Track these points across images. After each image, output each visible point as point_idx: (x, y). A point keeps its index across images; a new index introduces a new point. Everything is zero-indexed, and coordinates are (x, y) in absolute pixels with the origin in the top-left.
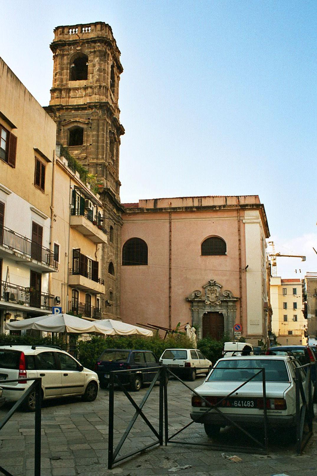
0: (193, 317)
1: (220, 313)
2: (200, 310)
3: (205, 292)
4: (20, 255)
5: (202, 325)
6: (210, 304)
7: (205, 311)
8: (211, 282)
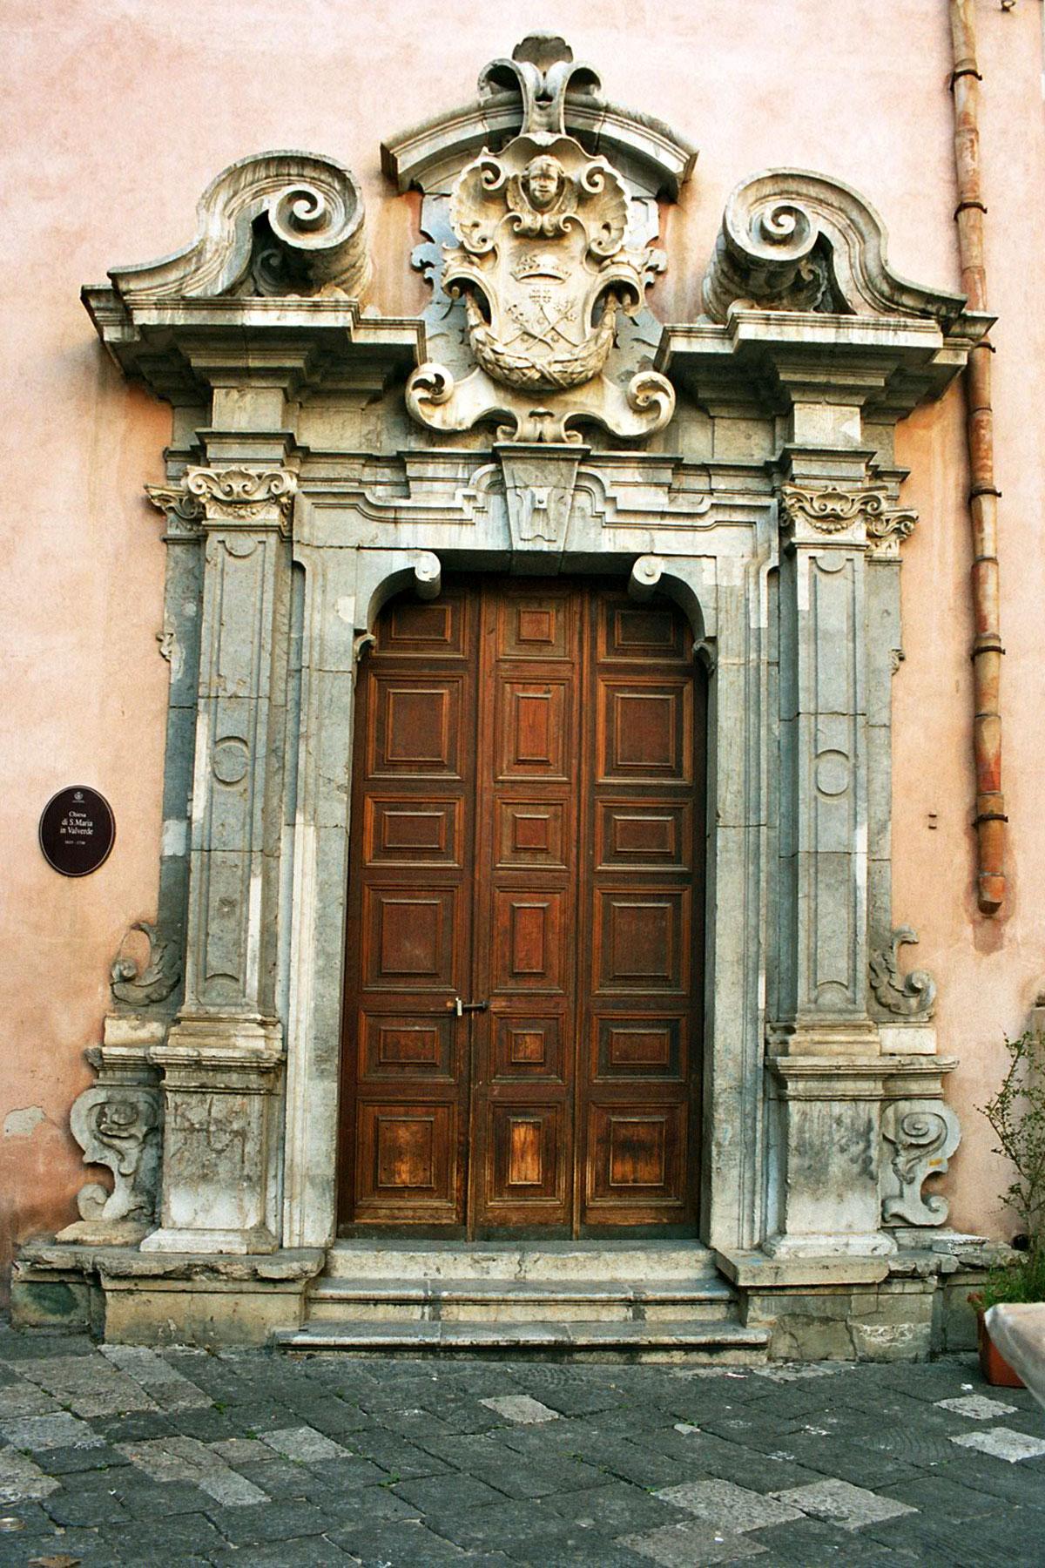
0: (192, 636)
1: (645, 573)
2: (316, 523)
3: (421, 252)
4: (283, 703)
5: (341, 774)
6: (489, 423)
7: (406, 534)
8: (529, 73)
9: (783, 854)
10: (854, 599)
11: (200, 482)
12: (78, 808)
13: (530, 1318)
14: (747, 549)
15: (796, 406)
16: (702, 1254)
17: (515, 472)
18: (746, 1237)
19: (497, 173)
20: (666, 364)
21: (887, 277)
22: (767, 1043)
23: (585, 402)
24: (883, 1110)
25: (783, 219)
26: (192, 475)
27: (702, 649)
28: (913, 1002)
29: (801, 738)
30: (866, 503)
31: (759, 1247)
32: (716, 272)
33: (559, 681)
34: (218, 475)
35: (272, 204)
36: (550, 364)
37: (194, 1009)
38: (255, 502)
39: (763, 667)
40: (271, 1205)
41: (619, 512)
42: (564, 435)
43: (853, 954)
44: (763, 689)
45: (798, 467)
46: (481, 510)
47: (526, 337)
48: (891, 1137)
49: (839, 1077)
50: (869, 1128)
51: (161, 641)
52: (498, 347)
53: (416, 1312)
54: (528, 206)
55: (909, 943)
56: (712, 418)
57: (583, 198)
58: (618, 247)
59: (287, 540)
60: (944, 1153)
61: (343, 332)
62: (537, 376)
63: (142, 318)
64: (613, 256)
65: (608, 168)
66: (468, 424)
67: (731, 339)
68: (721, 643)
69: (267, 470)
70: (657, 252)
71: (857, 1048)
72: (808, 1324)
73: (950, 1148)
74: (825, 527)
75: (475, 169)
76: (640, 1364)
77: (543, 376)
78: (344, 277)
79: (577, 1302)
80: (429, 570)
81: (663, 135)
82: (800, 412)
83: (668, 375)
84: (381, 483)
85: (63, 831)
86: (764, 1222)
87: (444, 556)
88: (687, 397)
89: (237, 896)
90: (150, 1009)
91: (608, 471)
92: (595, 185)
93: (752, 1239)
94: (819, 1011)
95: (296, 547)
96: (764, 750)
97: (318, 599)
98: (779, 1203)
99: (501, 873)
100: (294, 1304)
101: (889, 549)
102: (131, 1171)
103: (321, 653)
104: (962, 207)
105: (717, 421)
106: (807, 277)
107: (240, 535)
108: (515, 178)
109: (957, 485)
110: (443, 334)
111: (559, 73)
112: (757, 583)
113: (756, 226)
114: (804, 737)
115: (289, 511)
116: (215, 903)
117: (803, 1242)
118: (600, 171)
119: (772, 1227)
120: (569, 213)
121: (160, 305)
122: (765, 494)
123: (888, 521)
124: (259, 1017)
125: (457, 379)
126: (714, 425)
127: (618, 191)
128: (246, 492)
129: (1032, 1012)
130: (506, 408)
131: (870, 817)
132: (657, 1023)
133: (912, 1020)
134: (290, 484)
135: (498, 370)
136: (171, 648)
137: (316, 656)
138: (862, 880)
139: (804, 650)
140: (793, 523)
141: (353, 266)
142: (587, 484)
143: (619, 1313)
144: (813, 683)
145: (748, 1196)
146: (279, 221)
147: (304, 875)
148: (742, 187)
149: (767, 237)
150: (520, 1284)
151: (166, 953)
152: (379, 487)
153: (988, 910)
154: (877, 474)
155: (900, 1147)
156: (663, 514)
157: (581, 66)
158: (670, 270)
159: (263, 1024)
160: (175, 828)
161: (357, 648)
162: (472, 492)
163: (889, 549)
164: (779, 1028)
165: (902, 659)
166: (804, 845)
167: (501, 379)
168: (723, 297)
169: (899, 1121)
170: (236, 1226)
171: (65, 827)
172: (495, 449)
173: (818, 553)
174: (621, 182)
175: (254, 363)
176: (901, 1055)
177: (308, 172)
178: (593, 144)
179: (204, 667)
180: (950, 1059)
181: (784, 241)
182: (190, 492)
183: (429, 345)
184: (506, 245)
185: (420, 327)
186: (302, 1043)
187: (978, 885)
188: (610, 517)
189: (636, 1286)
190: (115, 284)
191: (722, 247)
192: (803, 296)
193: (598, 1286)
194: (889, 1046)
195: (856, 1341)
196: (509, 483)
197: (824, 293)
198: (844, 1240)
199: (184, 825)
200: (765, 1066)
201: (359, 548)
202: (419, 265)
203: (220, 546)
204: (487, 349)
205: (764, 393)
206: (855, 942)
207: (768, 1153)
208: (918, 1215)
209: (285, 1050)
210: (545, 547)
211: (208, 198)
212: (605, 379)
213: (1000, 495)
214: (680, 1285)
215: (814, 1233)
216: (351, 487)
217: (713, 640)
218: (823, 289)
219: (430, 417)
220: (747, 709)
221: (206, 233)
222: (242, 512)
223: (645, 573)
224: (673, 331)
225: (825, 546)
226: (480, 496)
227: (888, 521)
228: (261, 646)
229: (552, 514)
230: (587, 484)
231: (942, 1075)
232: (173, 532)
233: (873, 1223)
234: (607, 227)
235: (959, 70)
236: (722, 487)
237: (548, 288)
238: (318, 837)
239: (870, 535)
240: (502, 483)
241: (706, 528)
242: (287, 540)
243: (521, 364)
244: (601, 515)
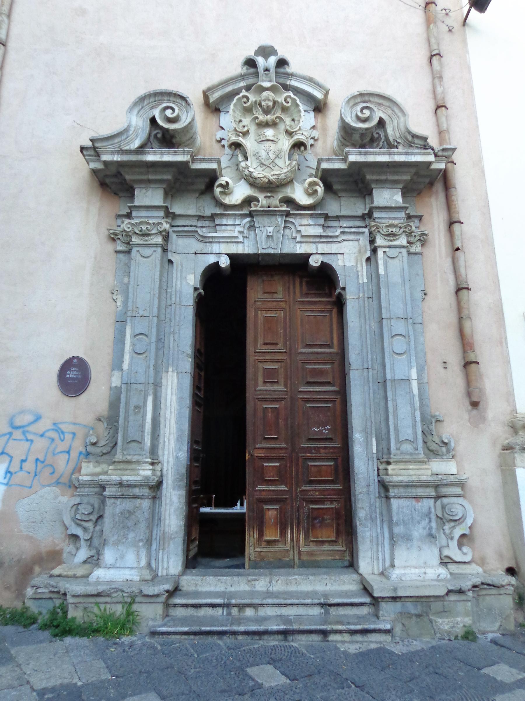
1: (314, 262)
6: (248, 201)
7: (215, 248)
8: (260, 61)
9: (380, 381)
10: (403, 269)
11: (129, 226)
12: (74, 366)
13: (274, 614)
14: (356, 250)
15: (374, 190)
16: (355, 576)
17: (257, 220)
18: (376, 568)
19: (248, 99)
20: (319, 175)
21: (409, 132)
22: (378, 469)
23: (288, 192)
24: (435, 502)
25: (364, 111)
26: (125, 223)
27: (340, 293)
28: (444, 449)
29: (384, 329)
30: (406, 228)
31: (382, 574)
32: (338, 136)
33: (280, 309)
34: (136, 223)
35: (156, 113)
36: (272, 176)
37: (121, 457)
38: (152, 234)
39: (366, 299)
40: (153, 553)
41: (302, 236)
42: (279, 205)
43: (414, 427)
44: (366, 309)
45: (376, 215)
46: (245, 237)
47: (262, 166)
48: (440, 515)
49: (415, 486)
50: (430, 512)
51: (113, 293)
52: (251, 169)
53: (219, 611)
54: (261, 112)
55: (439, 421)
56: (340, 197)
57: (284, 109)
58: (298, 128)
59: (165, 250)
60: (466, 524)
61: (186, 163)
62: (267, 180)
63: (105, 158)
64: (296, 131)
65: (292, 96)
66: (239, 202)
67: (346, 162)
68: (347, 289)
69: (156, 221)
70: (315, 132)
71: (422, 472)
72: (410, 618)
73: (469, 521)
74: (389, 238)
75: (240, 98)
76: (328, 641)
77: (269, 180)
78: (188, 143)
79: (297, 605)
80: (224, 262)
81: (315, 84)
82: (375, 193)
83: (321, 179)
84: (205, 227)
85: (68, 376)
86: (384, 560)
87: (231, 256)
88: (328, 188)
89: (141, 404)
90: (102, 457)
91: (297, 220)
92: (288, 103)
93: (378, 569)
94: (402, 453)
95: (170, 253)
96: (368, 335)
97: (179, 275)
98: (390, 550)
99: (258, 392)
100: (159, 609)
101: (417, 248)
102: (89, 538)
103: (180, 298)
104: (438, 107)
105: (341, 198)
106: (376, 136)
107: (145, 248)
108: (256, 101)
109: (444, 220)
110: (229, 167)
111: (272, 60)
112: (362, 265)
113: (354, 115)
114: (385, 329)
115: (166, 238)
116: (132, 408)
117: (403, 572)
118: (290, 97)
119: (388, 564)
120: (278, 115)
121: (113, 153)
122: (363, 227)
123: (415, 236)
124: (149, 460)
125: (235, 183)
127: (297, 105)
128: (149, 230)
129: (500, 453)
130: (256, 195)
131: (417, 364)
132: (328, 459)
133: (445, 457)
134: (166, 226)
135: (251, 179)
136: (117, 296)
137: (178, 299)
138: (415, 391)
139: (383, 291)
140: (375, 238)
141: (192, 138)
142: (289, 225)
143: (316, 611)
144: (388, 305)
145: (375, 546)
146: (160, 119)
147: (172, 394)
148: (347, 99)
149: (359, 119)
150: (269, 594)
151: (111, 431)
152: (204, 229)
153: (475, 405)
154: (409, 217)
155: (445, 521)
156: (321, 237)
157: (281, 57)
158: (320, 139)
159: (152, 464)
160: (117, 374)
161: (196, 295)
162: (242, 230)
163: (417, 248)
164: (383, 462)
165: (425, 294)
166: (389, 377)
167: (253, 183)
168: (342, 147)
169: (443, 507)
170: (135, 565)
171: (69, 374)
172: (251, 211)
173: (387, 250)
174: (298, 101)
175: (151, 177)
176: (441, 474)
177: (172, 99)
178: (287, 88)
179: (130, 304)
180: (464, 477)
181: (365, 120)
182: (125, 230)
183: (223, 171)
184: (253, 129)
185: (219, 162)
186: (170, 472)
187: (469, 394)
188: (299, 239)
189: (326, 595)
190: (93, 145)
191: (340, 125)
192: (375, 144)
193: (307, 595)
194: (435, 471)
195: (435, 627)
196: (257, 226)
197: (383, 142)
198: (423, 570)
199: (121, 373)
200: (379, 481)
201: (196, 254)
202: (219, 139)
203: (138, 253)
204: (246, 171)
205: (361, 185)
206: (415, 421)
207: (383, 524)
208: (457, 556)
209: (162, 476)
210: (272, 251)
211: (131, 109)
212: (294, 182)
213: (463, 223)
214: (346, 594)
215: (408, 566)
216: (194, 229)
217: (344, 289)
218: (383, 140)
219: (224, 199)
220: (360, 318)
221: (130, 123)
222: (147, 238)
223: (314, 262)
224: (322, 160)
225: (390, 247)
226: (246, 231)
227: (415, 236)
228: (154, 295)
229: (275, 238)
230: (289, 225)
231: (462, 485)
232: (119, 248)
233: (436, 561)
234: (293, 120)
235: (433, 53)
236: (345, 225)
237: (270, 145)
238: (178, 377)
239: (408, 242)
240: (254, 226)
242: (165, 250)
243: (260, 176)
244: (295, 238)
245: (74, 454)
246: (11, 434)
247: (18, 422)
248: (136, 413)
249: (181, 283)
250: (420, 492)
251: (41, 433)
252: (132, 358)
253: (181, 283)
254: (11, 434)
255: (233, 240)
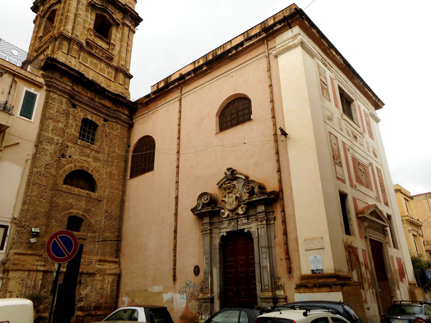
1: (246, 231)
7: (223, 231)
80: (225, 234)
87: (226, 232)
126: (335, 269)
184: (227, 194)
188: (241, 225)
225: (261, 225)
241: (251, 224)
245: (198, 291)
246: (186, 286)
247: (187, 284)
248: (207, 280)
249: (216, 242)
250: (269, 301)
251: (192, 286)
252: (205, 265)
253: (216, 242)
254: (186, 286)
255: (226, 228)
